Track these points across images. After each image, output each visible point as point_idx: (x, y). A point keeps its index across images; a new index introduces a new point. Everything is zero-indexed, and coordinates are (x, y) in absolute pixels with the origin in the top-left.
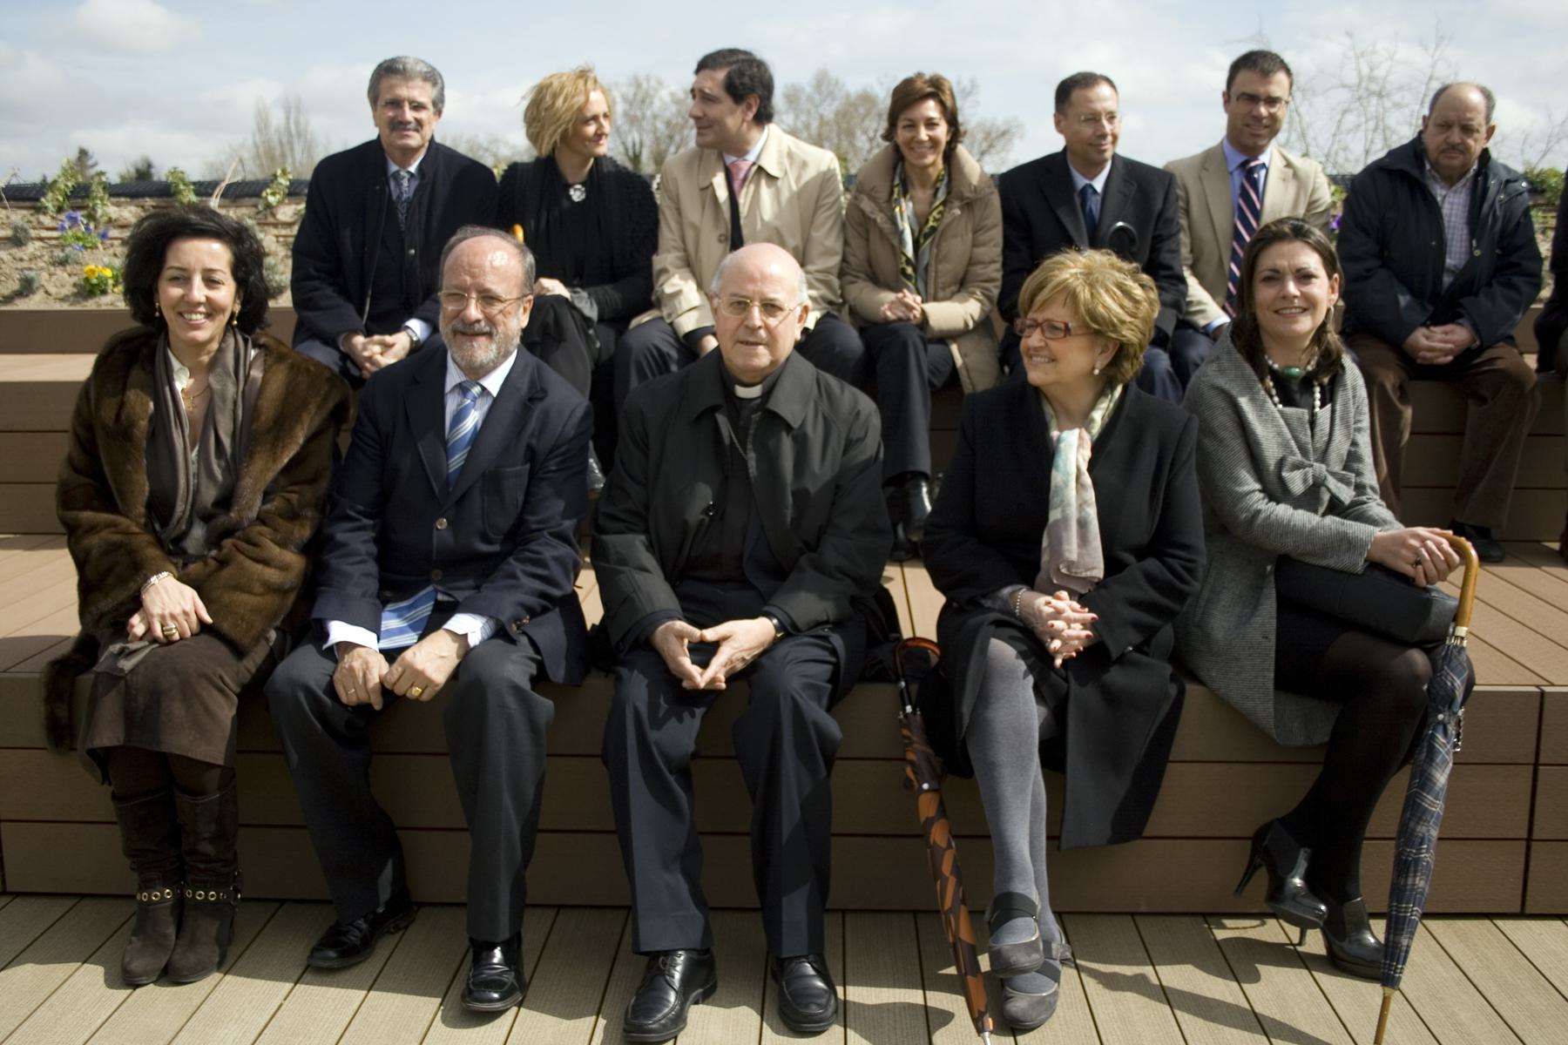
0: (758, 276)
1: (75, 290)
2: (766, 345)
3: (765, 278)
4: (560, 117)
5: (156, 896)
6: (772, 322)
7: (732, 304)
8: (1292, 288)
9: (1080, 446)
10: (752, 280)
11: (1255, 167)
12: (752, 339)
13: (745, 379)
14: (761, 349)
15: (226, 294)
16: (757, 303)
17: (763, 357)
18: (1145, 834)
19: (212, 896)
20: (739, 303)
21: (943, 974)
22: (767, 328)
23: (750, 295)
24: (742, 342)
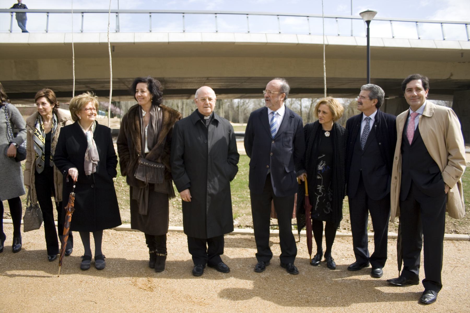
0: (207, 93)
1: (82, 259)
2: (210, 107)
3: (208, 93)
4: (150, 172)
6: (211, 102)
7: (202, 100)
8: (415, 93)
9: (91, 135)
10: (205, 94)
12: (207, 106)
14: (209, 108)
17: (209, 110)
20: (203, 99)
21: (206, 243)
22: (210, 104)
24: (205, 107)
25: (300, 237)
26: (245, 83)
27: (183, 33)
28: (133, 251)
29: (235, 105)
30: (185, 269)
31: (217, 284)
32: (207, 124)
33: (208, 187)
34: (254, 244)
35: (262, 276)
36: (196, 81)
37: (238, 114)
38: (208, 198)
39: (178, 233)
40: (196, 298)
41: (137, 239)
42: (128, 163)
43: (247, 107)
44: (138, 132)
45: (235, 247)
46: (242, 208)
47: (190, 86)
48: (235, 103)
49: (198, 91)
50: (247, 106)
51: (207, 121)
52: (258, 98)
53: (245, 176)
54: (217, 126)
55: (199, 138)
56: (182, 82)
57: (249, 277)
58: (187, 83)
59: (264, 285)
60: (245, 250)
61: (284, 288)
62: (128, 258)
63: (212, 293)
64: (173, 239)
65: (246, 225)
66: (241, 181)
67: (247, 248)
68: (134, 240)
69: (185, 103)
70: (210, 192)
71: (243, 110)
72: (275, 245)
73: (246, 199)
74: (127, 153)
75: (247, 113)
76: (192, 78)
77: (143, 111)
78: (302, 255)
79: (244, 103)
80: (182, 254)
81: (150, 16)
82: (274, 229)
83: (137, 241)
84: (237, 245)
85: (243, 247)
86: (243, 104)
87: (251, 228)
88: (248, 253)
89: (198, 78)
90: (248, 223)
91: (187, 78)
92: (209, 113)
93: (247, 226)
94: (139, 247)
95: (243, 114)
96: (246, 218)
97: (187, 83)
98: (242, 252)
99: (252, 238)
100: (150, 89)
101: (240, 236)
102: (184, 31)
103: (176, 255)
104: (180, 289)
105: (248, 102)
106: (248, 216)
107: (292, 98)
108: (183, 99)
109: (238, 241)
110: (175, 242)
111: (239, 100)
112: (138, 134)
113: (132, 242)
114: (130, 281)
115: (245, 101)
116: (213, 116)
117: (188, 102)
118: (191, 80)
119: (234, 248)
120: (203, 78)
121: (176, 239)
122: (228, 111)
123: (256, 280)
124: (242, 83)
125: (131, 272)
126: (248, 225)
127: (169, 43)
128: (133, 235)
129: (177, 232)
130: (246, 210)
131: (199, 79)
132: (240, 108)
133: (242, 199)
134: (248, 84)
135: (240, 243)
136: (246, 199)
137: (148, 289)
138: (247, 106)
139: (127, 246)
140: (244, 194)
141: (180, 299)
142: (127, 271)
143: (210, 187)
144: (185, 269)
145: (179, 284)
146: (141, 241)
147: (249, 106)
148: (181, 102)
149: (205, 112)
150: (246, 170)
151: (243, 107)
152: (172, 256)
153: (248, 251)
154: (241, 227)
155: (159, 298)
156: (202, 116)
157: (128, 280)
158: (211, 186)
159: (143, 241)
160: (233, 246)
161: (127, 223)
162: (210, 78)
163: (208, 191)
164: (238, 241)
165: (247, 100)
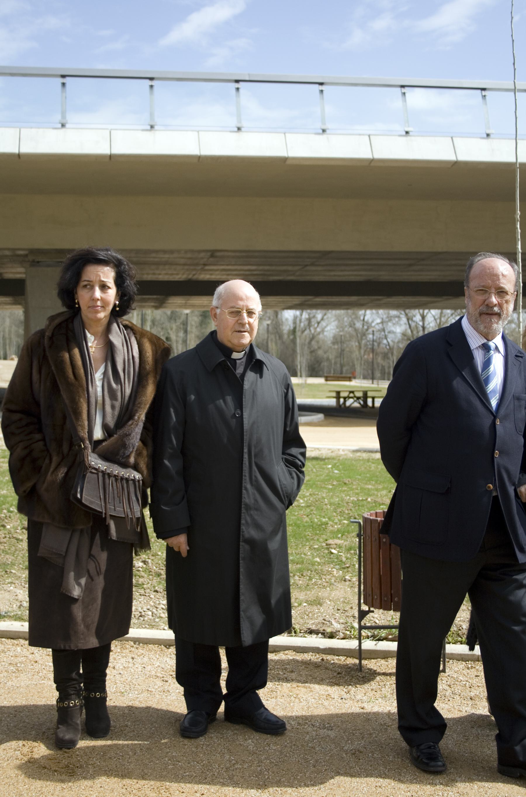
0: (244, 297)
2: (248, 332)
5: (72, 703)
10: (241, 299)
11: (116, 260)
12: (242, 330)
13: (238, 349)
15: (112, 293)
16: (245, 311)
17: (247, 339)
18: (393, 546)
19: (98, 695)
22: (249, 324)
23: (241, 307)
24: (236, 331)
25: (447, 660)
26: (313, 268)
27: (150, 130)
28: (22, 684)
29: (286, 328)
30: (155, 727)
31: (233, 762)
32: (240, 370)
33: (243, 522)
34: (327, 676)
35: (346, 748)
36: (182, 261)
37: (294, 351)
38: (244, 548)
39: (135, 646)
40: (182, 790)
41: (31, 656)
42: (47, 461)
43: (319, 333)
44: (82, 386)
45: (279, 680)
46: (300, 588)
47: (166, 274)
48: (287, 319)
49: (221, 289)
50: (318, 330)
51: (238, 361)
52: (348, 309)
53: (308, 510)
54: (261, 377)
55: (221, 401)
56: (145, 263)
57: (313, 748)
58: (158, 264)
59: (351, 768)
60: (304, 687)
61: (400, 775)
62: (10, 700)
63: (222, 780)
64: (123, 660)
65: (309, 629)
66: (299, 522)
67: (310, 683)
68: (23, 659)
69: (149, 318)
70: (247, 535)
71: (307, 341)
72: (382, 677)
73: (310, 567)
74: (38, 436)
75: (319, 348)
76: (172, 252)
77: (89, 335)
78: (449, 703)
79: (309, 320)
80: (145, 694)
81: (64, 84)
82: (379, 640)
83: (31, 661)
84: (286, 675)
85: (299, 681)
86: (306, 323)
87: (320, 635)
88: (311, 694)
89: (186, 252)
90: (313, 624)
91: (157, 252)
92: (243, 345)
93: (311, 632)
94: (35, 677)
95: (306, 351)
96: (309, 610)
97: (158, 264)
98: (298, 692)
99: (323, 660)
100: (119, 281)
101: (292, 656)
102: (152, 127)
103: (130, 695)
104: (143, 770)
105: (322, 319)
106: (315, 607)
107: (442, 308)
108: (144, 307)
109: (288, 666)
110: (128, 667)
111: (298, 313)
112: (84, 390)
113: (19, 665)
114: (17, 752)
115: (314, 317)
116: (251, 353)
117: (158, 317)
118: (167, 256)
119: (277, 683)
120: (200, 251)
121: (131, 660)
122: (267, 342)
123: (331, 756)
124: (307, 265)
125: (19, 732)
126: (314, 627)
127: (111, 157)
128: (19, 649)
129: (132, 643)
130: (308, 592)
131: (189, 255)
132: (298, 334)
133: (299, 566)
134: (319, 268)
135: (292, 672)
136: (310, 567)
137: (63, 770)
138: (318, 330)
139: (5, 674)
140: (305, 554)
141: (143, 792)
142: (8, 729)
143: (246, 521)
144: (155, 727)
145: (138, 760)
146: (40, 662)
147: (323, 331)
148: (138, 315)
149: (235, 341)
150: (310, 494)
151: (307, 332)
152: (121, 698)
153: (311, 691)
154: (295, 632)
155: (90, 789)
156: (227, 351)
157: (11, 749)
158: (249, 519)
159: (47, 664)
160: (274, 678)
161: (6, 619)
162: (218, 254)
163: (243, 532)
164: (288, 666)
165: (319, 314)
